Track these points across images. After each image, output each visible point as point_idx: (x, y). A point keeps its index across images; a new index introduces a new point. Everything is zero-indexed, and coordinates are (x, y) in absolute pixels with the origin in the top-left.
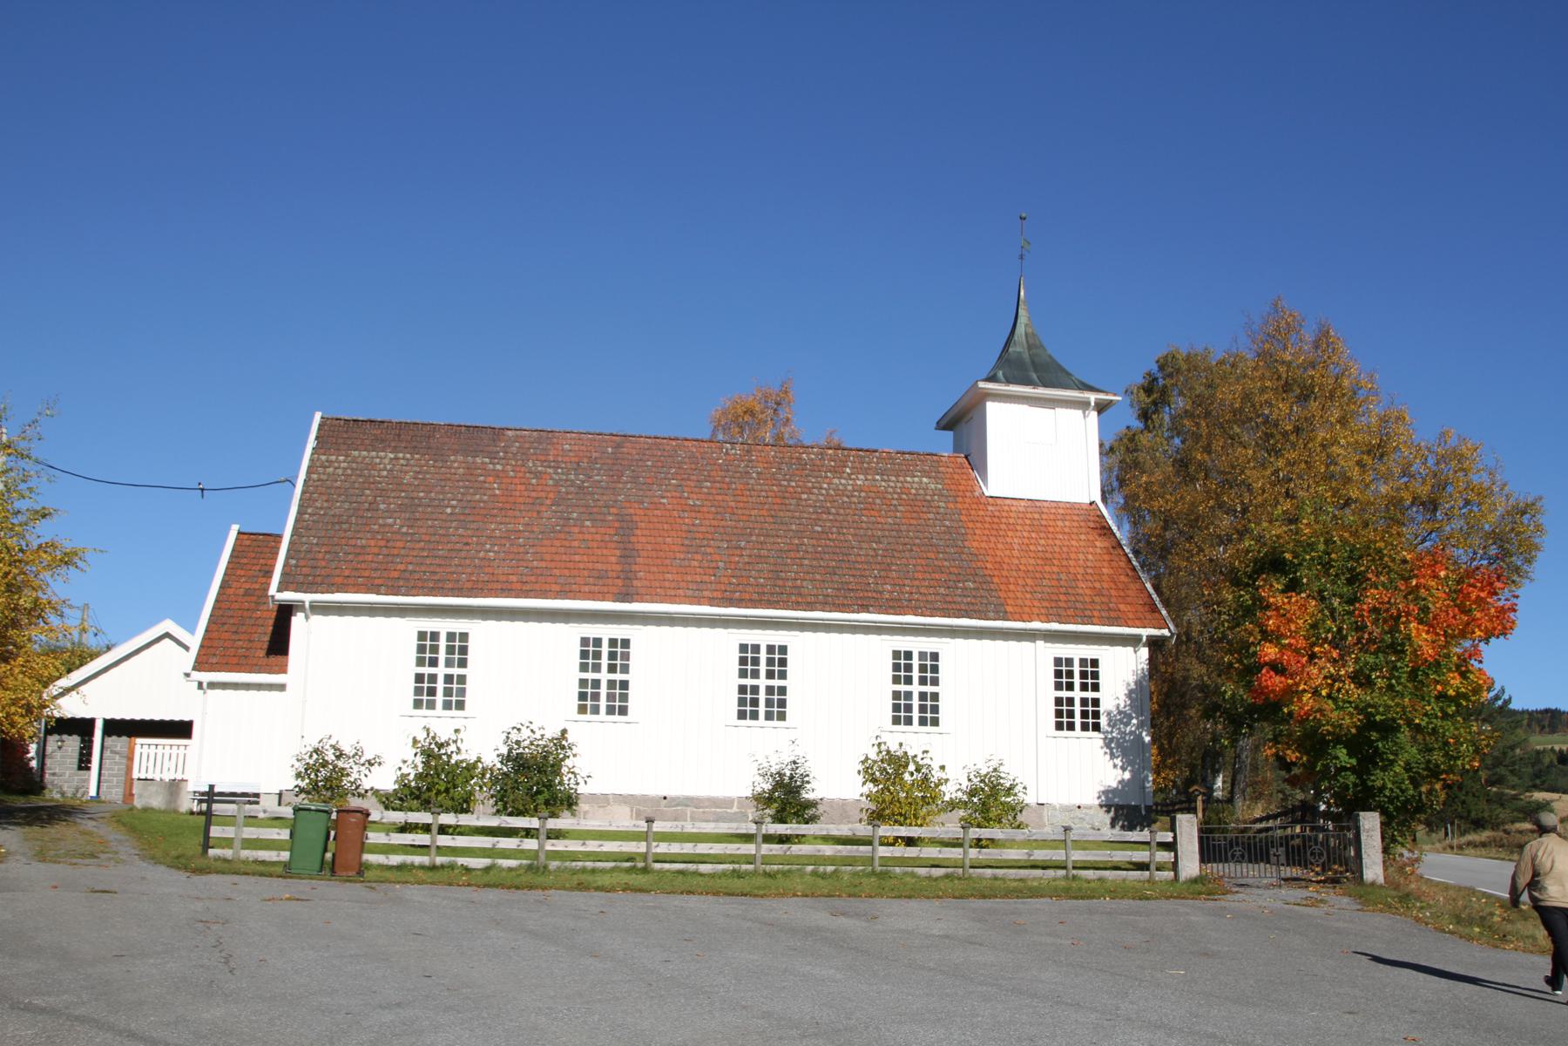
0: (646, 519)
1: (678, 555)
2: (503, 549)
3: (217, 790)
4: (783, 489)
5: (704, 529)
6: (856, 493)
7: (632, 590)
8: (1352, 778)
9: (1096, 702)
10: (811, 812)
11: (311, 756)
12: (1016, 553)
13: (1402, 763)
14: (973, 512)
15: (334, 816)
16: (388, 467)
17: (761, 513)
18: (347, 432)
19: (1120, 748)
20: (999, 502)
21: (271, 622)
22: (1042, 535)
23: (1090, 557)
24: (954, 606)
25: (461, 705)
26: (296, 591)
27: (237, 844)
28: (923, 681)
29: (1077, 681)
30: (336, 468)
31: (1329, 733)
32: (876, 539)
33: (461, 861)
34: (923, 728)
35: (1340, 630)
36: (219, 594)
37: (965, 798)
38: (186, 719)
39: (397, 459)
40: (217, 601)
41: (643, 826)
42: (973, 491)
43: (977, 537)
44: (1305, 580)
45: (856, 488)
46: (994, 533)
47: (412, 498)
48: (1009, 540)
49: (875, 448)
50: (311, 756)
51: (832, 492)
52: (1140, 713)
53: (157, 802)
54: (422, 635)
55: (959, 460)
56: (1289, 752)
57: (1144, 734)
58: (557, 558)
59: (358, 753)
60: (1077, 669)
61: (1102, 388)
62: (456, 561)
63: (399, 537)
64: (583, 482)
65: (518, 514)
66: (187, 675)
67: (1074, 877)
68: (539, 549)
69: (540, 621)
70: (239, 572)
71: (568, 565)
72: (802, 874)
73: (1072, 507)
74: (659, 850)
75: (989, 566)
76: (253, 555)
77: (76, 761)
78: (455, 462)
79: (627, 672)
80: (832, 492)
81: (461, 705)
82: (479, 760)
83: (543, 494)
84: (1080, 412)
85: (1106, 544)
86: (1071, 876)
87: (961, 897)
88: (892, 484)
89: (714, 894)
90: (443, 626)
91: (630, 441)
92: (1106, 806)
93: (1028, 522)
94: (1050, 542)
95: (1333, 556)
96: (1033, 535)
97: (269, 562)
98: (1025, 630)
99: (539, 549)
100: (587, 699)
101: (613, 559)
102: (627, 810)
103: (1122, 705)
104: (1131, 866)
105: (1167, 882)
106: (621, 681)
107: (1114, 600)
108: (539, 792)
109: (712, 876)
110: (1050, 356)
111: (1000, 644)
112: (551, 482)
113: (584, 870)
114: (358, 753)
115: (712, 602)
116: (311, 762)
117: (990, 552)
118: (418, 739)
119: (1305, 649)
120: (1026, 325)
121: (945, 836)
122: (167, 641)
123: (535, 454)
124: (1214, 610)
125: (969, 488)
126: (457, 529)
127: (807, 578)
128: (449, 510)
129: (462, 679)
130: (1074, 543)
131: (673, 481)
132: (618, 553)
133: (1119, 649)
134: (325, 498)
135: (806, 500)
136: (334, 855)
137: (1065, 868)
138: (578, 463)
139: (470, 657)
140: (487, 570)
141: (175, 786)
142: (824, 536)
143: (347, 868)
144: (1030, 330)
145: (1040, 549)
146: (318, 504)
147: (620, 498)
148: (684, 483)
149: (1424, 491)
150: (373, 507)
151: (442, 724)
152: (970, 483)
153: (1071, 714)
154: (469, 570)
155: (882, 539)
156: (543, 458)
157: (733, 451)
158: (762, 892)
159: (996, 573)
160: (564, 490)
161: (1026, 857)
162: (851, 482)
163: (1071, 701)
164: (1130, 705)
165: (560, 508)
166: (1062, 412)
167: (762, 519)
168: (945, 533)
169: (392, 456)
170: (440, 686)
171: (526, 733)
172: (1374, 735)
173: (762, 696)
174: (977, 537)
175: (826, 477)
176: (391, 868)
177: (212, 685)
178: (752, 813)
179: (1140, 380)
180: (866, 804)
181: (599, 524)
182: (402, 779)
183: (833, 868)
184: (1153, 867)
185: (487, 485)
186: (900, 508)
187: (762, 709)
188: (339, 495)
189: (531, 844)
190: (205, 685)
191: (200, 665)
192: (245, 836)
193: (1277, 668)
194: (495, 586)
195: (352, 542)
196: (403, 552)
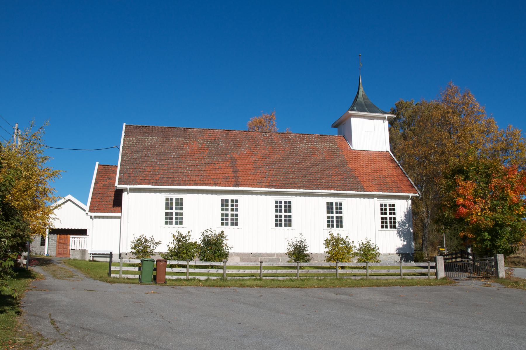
0: (240, 158)
1: (252, 171)
2: (193, 169)
4: (284, 148)
5: (259, 162)
7: (238, 183)
8: (489, 243)
9: (394, 219)
10: (308, 258)
12: (364, 169)
13: (506, 237)
14: (348, 155)
16: (150, 142)
17: (278, 156)
18: (135, 130)
19: (402, 234)
20: (356, 151)
21: (113, 195)
22: (372, 162)
23: (389, 170)
25: (181, 223)
26: (124, 184)
27: (121, 272)
28: (337, 213)
29: (388, 211)
30: (133, 142)
33: (197, 277)
34: (337, 229)
35: (485, 193)
36: (95, 186)
37: (358, 252)
38: (86, 229)
39: (152, 139)
40: (94, 188)
41: (259, 264)
42: (347, 148)
43: (351, 164)
44: (471, 176)
45: (308, 147)
46: (356, 162)
48: (361, 164)
51: (301, 149)
52: (409, 222)
53: (78, 257)
54: (167, 199)
55: (341, 138)
56: (469, 234)
57: (411, 229)
58: (212, 172)
60: (388, 208)
61: (386, 111)
64: (217, 146)
67: (403, 278)
68: (205, 169)
69: (212, 194)
70: (100, 178)
71: (215, 174)
72: (313, 279)
73: (381, 153)
74: (264, 273)
75: (356, 173)
76: (104, 172)
77: (40, 243)
79: (238, 211)
80: (301, 149)
81: (181, 223)
84: (382, 121)
85: (394, 165)
86: (402, 278)
87: (370, 286)
88: (320, 146)
89: (287, 287)
90: (174, 196)
92: (398, 253)
93: (367, 158)
94: (375, 165)
95: (480, 168)
96: (369, 162)
98: (371, 195)
99: (205, 169)
100: (224, 221)
101: (231, 172)
102: (239, 258)
103: (403, 220)
104: (419, 274)
107: (399, 184)
108: (216, 253)
109: (283, 281)
110: (371, 102)
112: (206, 146)
115: (266, 187)
117: (356, 168)
118: (175, 235)
119: (472, 200)
120: (362, 92)
121: (353, 266)
122: (69, 202)
124: (439, 187)
125: (346, 147)
126: (176, 163)
127: (297, 178)
130: (383, 165)
132: (232, 170)
133: (402, 201)
134: (130, 152)
135: (292, 151)
137: (400, 275)
138: (214, 140)
139: (184, 206)
140: (188, 176)
141: (84, 252)
142: (300, 164)
143: (160, 281)
144: (364, 94)
146: (128, 155)
147: (230, 152)
148: (251, 146)
149: (503, 146)
151: (336, 232)
152: (346, 145)
154: (182, 177)
157: (266, 135)
158: (303, 286)
159: (359, 175)
160: (211, 149)
161: (387, 272)
162: (306, 145)
163: (386, 218)
164: (406, 219)
166: (376, 121)
167: (278, 158)
168: (340, 162)
169: (151, 138)
171: (209, 232)
172: (498, 228)
173: (283, 219)
174: (351, 164)
175: (298, 144)
176: (174, 280)
177: (96, 217)
178: (288, 258)
180: (327, 255)
181: (224, 160)
183: (323, 277)
184: (429, 274)
186: (324, 154)
188: (135, 152)
189: (221, 271)
190: (93, 217)
191: (91, 210)
192: (123, 270)
193: (463, 206)
194: (192, 182)
195: (141, 167)
196: (159, 171)
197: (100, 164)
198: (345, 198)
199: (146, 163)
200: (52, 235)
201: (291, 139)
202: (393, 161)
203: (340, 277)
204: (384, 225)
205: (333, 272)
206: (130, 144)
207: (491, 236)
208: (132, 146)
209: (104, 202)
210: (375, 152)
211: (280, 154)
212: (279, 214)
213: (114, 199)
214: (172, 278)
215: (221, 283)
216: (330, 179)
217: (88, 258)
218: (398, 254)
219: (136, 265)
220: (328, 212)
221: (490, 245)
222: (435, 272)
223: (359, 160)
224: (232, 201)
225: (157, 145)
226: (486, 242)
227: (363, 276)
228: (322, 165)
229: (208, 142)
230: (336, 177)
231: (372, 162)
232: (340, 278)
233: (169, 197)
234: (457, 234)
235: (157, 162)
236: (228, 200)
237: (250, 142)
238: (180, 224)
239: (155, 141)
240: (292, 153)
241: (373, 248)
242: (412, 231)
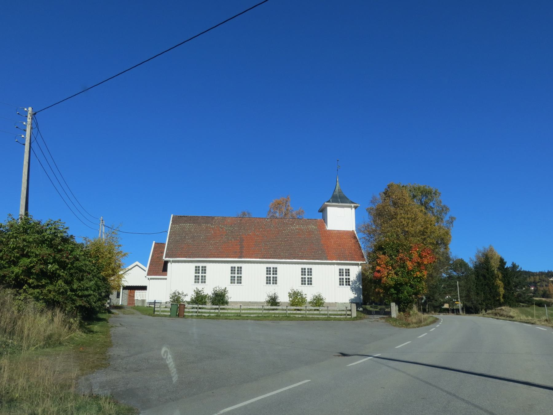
1: (253, 247)
3: (156, 302)
5: (259, 240)
6: (296, 230)
9: (349, 279)
11: (173, 294)
14: (323, 234)
15: (178, 306)
16: (188, 228)
19: (354, 289)
21: (163, 264)
24: (315, 257)
25: (205, 282)
27: (160, 311)
28: (308, 275)
31: (388, 286)
33: (203, 314)
47: (193, 235)
50: (173, 294)
51: (290, 230)
53: (140, 304)
54: (196, 267)
59: (183, 293)
61: (355, 202)
62: (203, 250)
63: (191, 245)
64: (232, 230)
65: (217, 238)
66: (146, 277)
67: (329, 317)
70: (155, 253)
71: (228, 250)
72: (271, 316)
74: (242, 312)
75: (325, 247)
78: (203, 226)
79: (241, 274)
80: (290, 230)
81: (205, 282)
82: (207, 294)
83: (223, 233)
84: (350, 209)
91: (244, 219)
95: (394, 246)
97: (162, 250)
100: (233, 280)
101: (238, 248)
103: (355, 279)
105: (349, 318)
107: (354, 255)
109: (253, 317)
110: (344, 195)
111: (326, 266)
113: (227, 316)
114: (183, 293)
115: (260, 258)
116: (173, 295)
122: (137, 266)
123: (222, 223)
128: (202, 238)
129: (205, 276)
134: (174, 236)
136: (179, 314)
140: (210, 252)
141: (143, 301)
144: (339, 188)
145: (338, 243)
146: (173, 237)
150: (185, 237)
151: (200, 286)
153: (343, 282)
154: (206, 252)
156: (223, 224)
165: (227, 236)
169: (189, 225)
170: (200, 278)
175: (289, 226)
176: (189, 316)
177: (151, 279)
179: (384, 191)
181: (235, 240)
182: (192, 299)
185: (210, 231)
186: (306, 234)
187: (272, 282)
188: (177, 235)
189: (217, 311)
191: (148, 274)
192: (162, 310)
197: (157, 242)
198: (279, 264)
199: (184, 243)
200: (125, 290)
204: (341, 283)
207: (397, 291)
212: (269, 276)
213: (163, 267)
214: (189, 315)
215: (217, 318)
217: (146, 305)
223: (330, 237)
224: (238, 268)
234: (484, 289)
238: (198, 283)
242: (361, 287)
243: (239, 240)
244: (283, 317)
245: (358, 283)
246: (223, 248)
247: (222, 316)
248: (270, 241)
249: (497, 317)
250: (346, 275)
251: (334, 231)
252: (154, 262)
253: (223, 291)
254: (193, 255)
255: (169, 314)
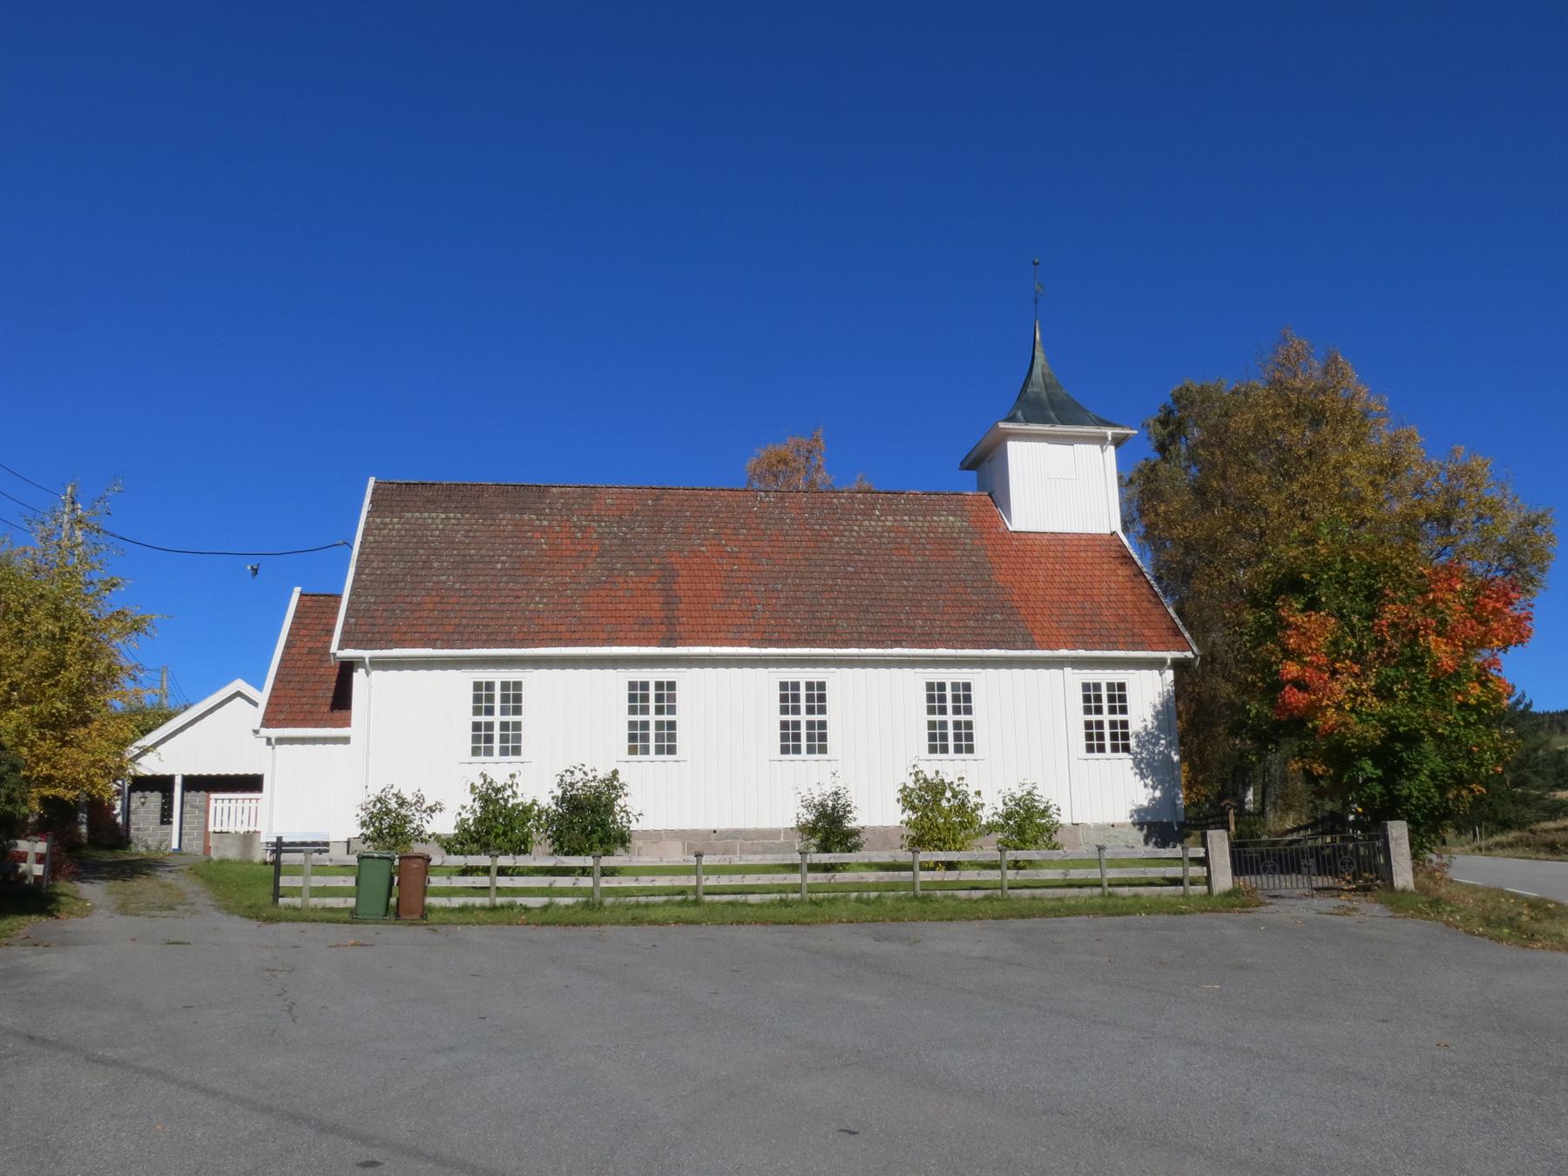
0: (687, 566)
1: (718, 600)
4: (816, 532)
7: (675, 635)
8: (1379, 788)
9: (1125, 724)
11: (374, 806)
12: (1041, 585)
13: (1427, 772)
14: (998, 547)
15: (397, 862)
16: (440, 527)
19: (1149, 768)
21: (334, 679)
22: (1066, 566)
23: (1113, 585)
25: (517, 751)
27: (306, 893)
28: (957, 711)
29: (1105, 704)
30: (390, 530)
32: (907, 577)
33: (520, 900)
38: (259, 773)
39: (448, 518)
41: (692, 860)
44: (1323, 599)
46: (1019, 566)
48: (1034, 572)
49: (902, 490)
50: (374, 806)
53: (232, 853)
56: (1315, 765)
57: (1173, 753)
58: (603, 607)
59: (420, 800)
60: (1104, 693)
61: (1108, 419)
62: (508, 614)
63: (452, 593)
64: (626, 534)
65: (564, 566)
66: (256, 732)
67: (1110, 895)
70: (302, 632)
71: (614, 613)
72: (847, 901)
74: (709, 883)
75: (1015, 598)
76: (315, 615)
81: (517, 751)
82: (534, 803)
83: (588, 547)
84: (1097, 448)
85: (1128, 573)
86: (1106, 893)
87: (1001, 918)
88: (920, 524)
90: (497, 676)
91: (669, 494)
92: (1138, 824)
95: (1351, 574)
100: (637, 740)
101: (657, 606)
103: (1150, 726)
106: (513, 723)
107: (1137, 625)
108: (593, 831)
109: (761, 906)
110: (1067, 395)
111: (1029, 672)
112: (595, 536)
113: (638, 905)
116: (375, 811)
117: (1016, 584)
118: (476, 785)
120: (1043, 366)
122: (239, 699)
124: (1236, 631)
126: (508, 583)
128: (499, 566)
130: (1097, 572)
131: (711, 530)
132: (661, 600)
135: (838, 542)
136: (398, 899)
137: (1100, 885)
138: (620, 516)
139: (524, 704)
141: (248, 838)
144: (1046, 371)
146: (374, 565)
147: (661, 548)
149: (1437, 507)
150: (426, 564)
151: (498, 769)
152: (994, 519)
154: (520, 622)
155: (912, 577)
157: (767, 499)
159: (1022, 604)
163: (1100, 724)
170: (497, 733)
171: (579, 775)
172: (1398, 746)
175: (857, 520)
176: (453, 910)
177: (280, 741)
179: (1158, 414)
184: (1186, 882)
186: (928, 546)
187: (804, 743)
188: (395, 555)
189: (586, 882)
190: (273, 740)
193: (1300, 685)
195: (409, 600)
196: (457, 607)
197: (307, 593)
198: (979, 670)
199: (422, 586)
200: (193, 793)
201: (837, 508)
202: (1127, 560)
203: (925, 892)
204: (1094, 741)
205: (903, 877)
206: (384, 536)
207: (1383, 770)
208: (387, 539)
209: (306, 699)
210: (1076, 537)
211: (801, 550)
212: (790, 718)
214: (448, 905)
215: (586, 915)
216: (937, 617)
218: (1140, 824)
219: (510, 871)
220: (931, 711)
221: (1382, 795)
222: (1206, 875)
223: (1028, 560)
224: (659, 685)
225: (459, 537)
226: (1368, 787)
227: (991, 889)
228: (920, 577)
229: (603, 524)
230: (957, 610)
231: (1066, 566)
232: (923, 894)
233: (484, 680)
235: (454, 583)
236: (493, 683)
237: (719, 520)
239: (454, 524)
240: (836, 545)
241: (1042, 807)
243: (658, 573)
244: (898, 899)
245: (1163, 742)
246: (592, 606)
247: (613, 905)
248: (787, 578)
249: (1559, 857)
250: (1112, 710)
251: (1038, 536)
252: (296, 671)
253: (603, 788)
254: (461, 633)
255: (351, 902)
